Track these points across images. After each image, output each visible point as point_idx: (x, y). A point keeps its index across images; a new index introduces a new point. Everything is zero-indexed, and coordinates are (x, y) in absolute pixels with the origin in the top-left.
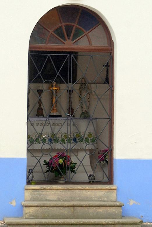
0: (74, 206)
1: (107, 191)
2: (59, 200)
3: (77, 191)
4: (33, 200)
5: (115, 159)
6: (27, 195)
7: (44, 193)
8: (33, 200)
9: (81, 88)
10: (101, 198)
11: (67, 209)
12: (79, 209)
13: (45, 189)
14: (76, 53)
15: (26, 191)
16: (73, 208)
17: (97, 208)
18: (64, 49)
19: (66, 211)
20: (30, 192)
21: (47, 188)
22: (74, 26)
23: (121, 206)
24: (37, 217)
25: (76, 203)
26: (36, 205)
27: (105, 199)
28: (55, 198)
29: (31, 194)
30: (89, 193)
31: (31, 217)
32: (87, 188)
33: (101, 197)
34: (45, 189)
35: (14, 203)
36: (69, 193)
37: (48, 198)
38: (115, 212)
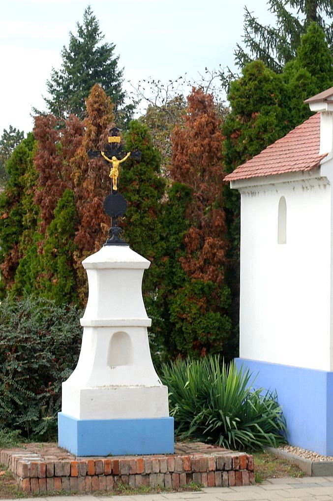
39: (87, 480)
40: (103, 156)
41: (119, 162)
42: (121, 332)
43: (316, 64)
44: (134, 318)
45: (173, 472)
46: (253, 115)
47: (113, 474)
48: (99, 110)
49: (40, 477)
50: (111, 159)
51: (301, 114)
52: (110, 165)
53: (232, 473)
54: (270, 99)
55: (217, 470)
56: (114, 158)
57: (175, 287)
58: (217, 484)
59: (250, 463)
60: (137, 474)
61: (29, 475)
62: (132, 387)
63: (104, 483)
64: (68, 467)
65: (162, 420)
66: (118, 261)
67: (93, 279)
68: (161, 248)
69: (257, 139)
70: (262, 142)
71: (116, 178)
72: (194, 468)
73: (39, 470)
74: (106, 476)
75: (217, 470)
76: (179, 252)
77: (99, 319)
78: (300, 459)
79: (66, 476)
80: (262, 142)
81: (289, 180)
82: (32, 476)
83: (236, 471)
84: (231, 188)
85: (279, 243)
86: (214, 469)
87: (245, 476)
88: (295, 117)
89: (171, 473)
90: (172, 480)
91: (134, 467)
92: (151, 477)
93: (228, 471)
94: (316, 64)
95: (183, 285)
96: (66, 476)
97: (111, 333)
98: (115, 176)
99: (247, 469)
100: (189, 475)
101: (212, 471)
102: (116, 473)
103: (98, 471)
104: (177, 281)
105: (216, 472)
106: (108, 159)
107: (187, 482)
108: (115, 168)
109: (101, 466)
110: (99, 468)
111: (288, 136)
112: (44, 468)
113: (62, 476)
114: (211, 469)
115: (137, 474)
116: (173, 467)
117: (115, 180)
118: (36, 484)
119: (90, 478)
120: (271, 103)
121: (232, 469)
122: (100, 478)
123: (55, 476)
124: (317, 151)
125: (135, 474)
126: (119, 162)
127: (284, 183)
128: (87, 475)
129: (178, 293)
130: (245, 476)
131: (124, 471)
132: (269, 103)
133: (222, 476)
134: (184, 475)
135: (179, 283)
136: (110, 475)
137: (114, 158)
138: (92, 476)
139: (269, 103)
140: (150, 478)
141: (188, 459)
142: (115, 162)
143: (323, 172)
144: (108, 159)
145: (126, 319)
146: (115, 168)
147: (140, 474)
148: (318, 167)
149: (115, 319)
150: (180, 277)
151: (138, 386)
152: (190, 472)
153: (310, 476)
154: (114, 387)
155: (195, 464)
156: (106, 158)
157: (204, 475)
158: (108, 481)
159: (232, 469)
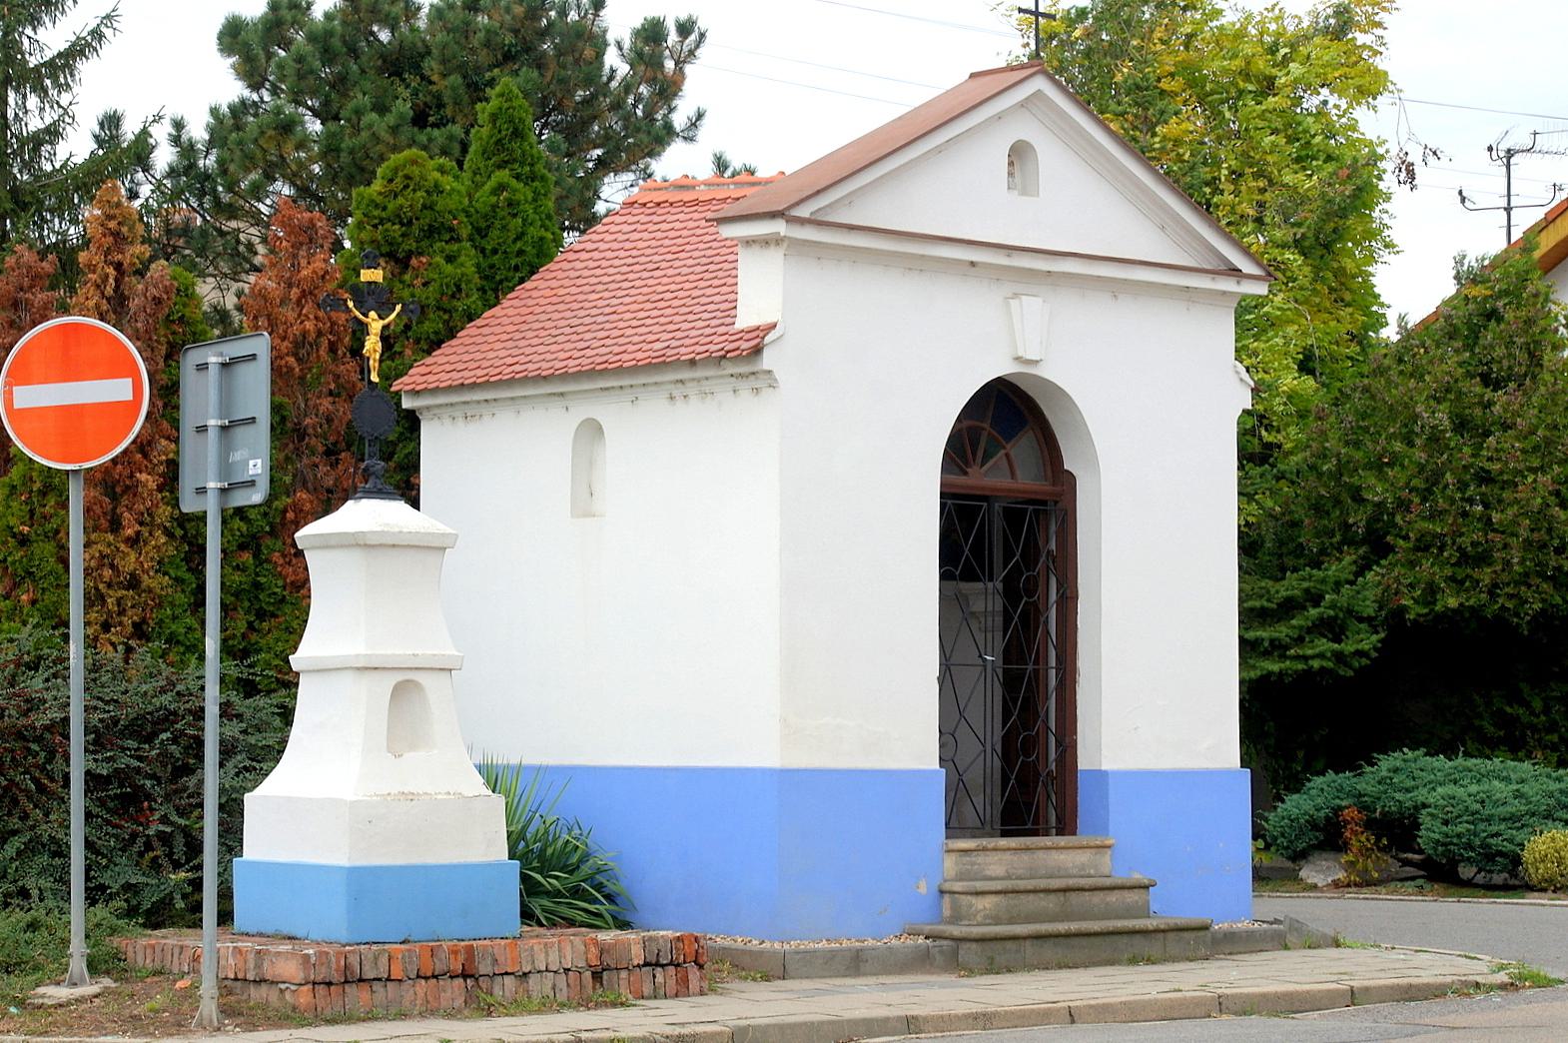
0: (1065, 890)
1: (1093, 851)
2: (1008, 877)
3: (1041, 854)
4: (960, 878)
5: (1101, 776)
6: (950, 864)
7: (980, 859)
8: (960, 878)
9: (15, 584)
10: (1084, 869)
11: (1052, 897)
12: (1073, 897)
13: (985, 849)
14: (1044, 503)
15: (946, 855)
16: (1062, 894)
17: (1106, 892)
18: (972, 488)
19: (1050, 903)
20: (953, 856)
21: (989, 846)
22: (983, 429)
23: (1147, 887)
24: (997, 921)
25: (1071, 882)
26: (999, 888)
27: (1092, 872)
28: (999, 871)
29: (956, 863)
30: (1062, 857)
31: (987, 921)
32: (1062, 844)
33: (1083, 867)
34: (985, 849)
35: (923, 889)
36: (1025, 857)
37: (988, 873)
38: (1137, 902)
39: (417, 988)
40: (351, 311)
41: (381, 323)
42: (408, 681)
43: (522, 164)
44: (435, 652)
45: (569, 970)
46: (414, 262)
47: (465, 976)
48: (116, 235)
49: (334, 981)
50: (366, 315)
51: (513, 263)
52: (361, 330)
53: (671, 969)
54: (451, 229)
55: (646, 964)
56: (373, 314)
57: (261, 615)
58: (645, 994)
59: (700, 951)
60: (507, 973)
61: (312, 977)
62: (439, 797)
63: (449, 994)
64: (384, 960)
65: (1228, 772)
66: (405, 530)
67: (317, 565)
68: (238, 533)
69: (438, 308)
70: (446, 317)
71: (378, 357)
72: (608, 960)
73: (334, 966)
74: (451, 977)
75: (646, 964)
76: (269, 541)
77: (369, 652)
78: (734, 946)
79: (380, 980)
80: (446, 317)
81: (633, 382)
82: (319, 979)
83: (678, 965)
84: (404, 407)
85: (572, 516)
86: (641, 963)
87: (694, 974)
88: (499, 269)
89: (567, 970)
90: (568, 985)
91: (501, 959)
92: (533, 979)
93: (663, 966)
94: (522, 164)
95: (279, 613)
96: (380, 980)
97: (391, 680)
98: (375, 351)
99: (695, 962)
100: (597, 976)
101: (638, 966)
102: (470, 973)
103: (439, 968)
104: (269, 603)
105: (644, 969)
106: (361, 317)
107: (594, 988)
108: (376, 335)
109: (443, 956)
110: (441, 960)
111: (505, 303)
112: (343, 963)
113: (374, 979)
114: (636, 963)
115: (507, 973)
116: (569, 958)
117: (375, 360)
118: (325, 997)
119: (423, 981)
120: (452, 239)
121: (671, 964)
122: (441, 982)
123: (361, 980)
124: (728, 320)
125: (502, 974)
126: (381, 323)
127: (550, 394)
128: (418, 976)
129: (270, 630)
130: (694, 974)
131: (484, 968)
132: (447, 237)
133: (654, 976)
134: (588, 974)
135: (272, 609)
136: (458, 976)
137: (373, 314)
138: (426, 978)
139: (447, 237)
140: (530, 982)
141: (596, 942)
142: (375, 324)
143: (768, 360)
144: (361, 317)
145: (420, 652)
146: (376, 335)
147: (512, 974)
148: (757, 351)
149: (389, 652)
150: (275, 593)
151: (449, 793)
152: (599, 969)
153: (779, 978)
154: (411, 797)
155: (608, 952)
156: (357, 313)
157: (624, 974)
158: (454, 990)
159: (671, 964)
